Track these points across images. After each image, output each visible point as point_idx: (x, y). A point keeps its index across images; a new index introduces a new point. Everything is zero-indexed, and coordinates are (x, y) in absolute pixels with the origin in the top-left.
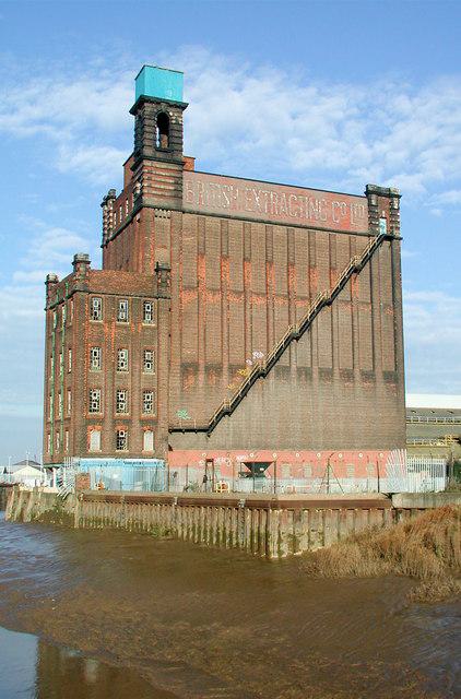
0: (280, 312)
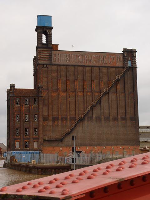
0: (89, 98)
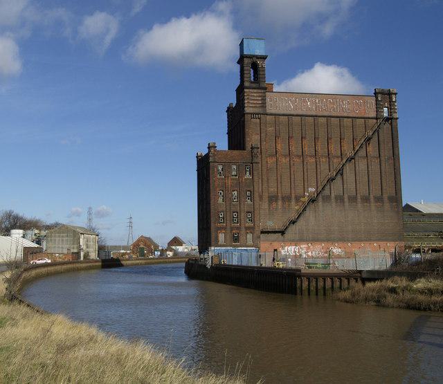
0: (324, 166)
